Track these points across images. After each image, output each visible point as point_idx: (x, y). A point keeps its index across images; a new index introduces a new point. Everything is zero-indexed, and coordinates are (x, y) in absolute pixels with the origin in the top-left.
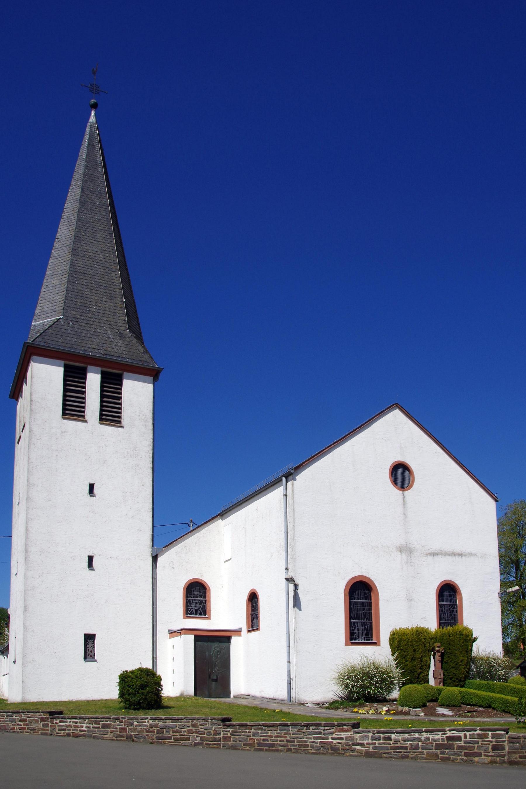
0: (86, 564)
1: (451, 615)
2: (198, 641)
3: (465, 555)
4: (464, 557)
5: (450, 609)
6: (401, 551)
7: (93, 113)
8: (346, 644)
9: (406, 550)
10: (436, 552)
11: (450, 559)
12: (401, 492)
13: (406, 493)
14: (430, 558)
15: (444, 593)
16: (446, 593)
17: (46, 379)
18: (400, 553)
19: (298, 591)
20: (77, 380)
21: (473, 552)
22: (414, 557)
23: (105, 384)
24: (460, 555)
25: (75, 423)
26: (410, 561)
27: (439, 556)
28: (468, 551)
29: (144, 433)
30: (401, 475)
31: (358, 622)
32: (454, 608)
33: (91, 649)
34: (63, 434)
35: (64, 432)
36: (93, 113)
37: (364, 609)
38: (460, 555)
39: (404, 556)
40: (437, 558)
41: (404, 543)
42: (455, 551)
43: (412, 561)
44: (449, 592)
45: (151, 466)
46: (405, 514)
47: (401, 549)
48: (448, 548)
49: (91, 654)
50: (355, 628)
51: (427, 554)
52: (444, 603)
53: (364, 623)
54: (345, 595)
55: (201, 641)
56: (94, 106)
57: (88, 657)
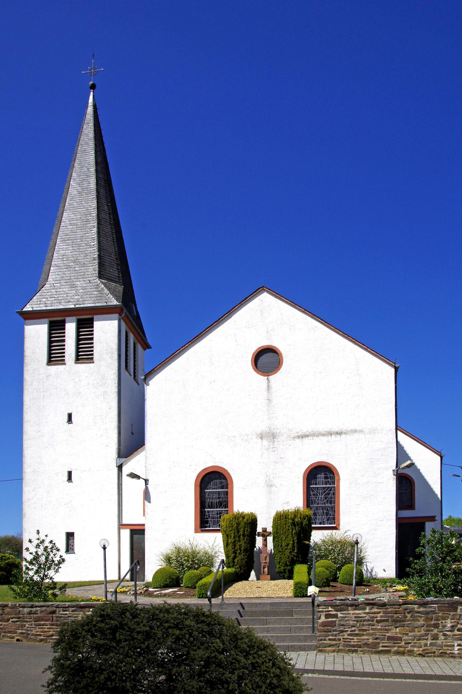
0: (66, 478)
1: (326, 498)
2: (135, 534)
3: (345, 433)
4: (343, 436)
5: (324, 492)
6: (261, 438)
7: (92, 93)
8: (196, 531)
9: (270, 436)
10: (307, 433)
11: (324, 439)
12: (266, 377)
13: (271, 377)
14: (297, 441)
15: (319, 476)
16: (321, 476)
17: (36, 335)
18: (260, 440)
19: (148, 486)
20: (59, 331)
21: (358, 429)
22: (278, 441)
23: (80, 330)
24: (339, 433)
25: (56, 367)
26: (272, 447)
27: (309, 438)
28: (352, 428)
29: (111, 364)
30: (266, 360)
31: (212, 511)
32: (330, 490)
33: (72, 544)
34: (48, 378)
35: (49, 376)
36: (92, 93)
37: (219, 498)
38: (339, 433)
39: (265, 442)
40: (306, 440)
41: (267, 429)
42: (332, 430)
43: (275, 446)
44: (325, 474)
45: (117, 390)
46: (269, 400)
47: (262, 436)
48: (322, 428)
49: (72, 548)
50: (209, 516)
51: (294, 438)
52: (318, 486)
53: (219, 511)
54: (195, 486)
55: (138, 534)
56: (93, 87)
57: (70, 550)
